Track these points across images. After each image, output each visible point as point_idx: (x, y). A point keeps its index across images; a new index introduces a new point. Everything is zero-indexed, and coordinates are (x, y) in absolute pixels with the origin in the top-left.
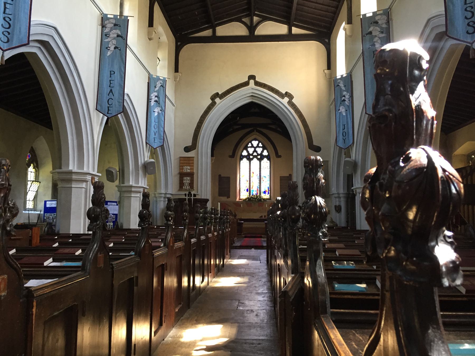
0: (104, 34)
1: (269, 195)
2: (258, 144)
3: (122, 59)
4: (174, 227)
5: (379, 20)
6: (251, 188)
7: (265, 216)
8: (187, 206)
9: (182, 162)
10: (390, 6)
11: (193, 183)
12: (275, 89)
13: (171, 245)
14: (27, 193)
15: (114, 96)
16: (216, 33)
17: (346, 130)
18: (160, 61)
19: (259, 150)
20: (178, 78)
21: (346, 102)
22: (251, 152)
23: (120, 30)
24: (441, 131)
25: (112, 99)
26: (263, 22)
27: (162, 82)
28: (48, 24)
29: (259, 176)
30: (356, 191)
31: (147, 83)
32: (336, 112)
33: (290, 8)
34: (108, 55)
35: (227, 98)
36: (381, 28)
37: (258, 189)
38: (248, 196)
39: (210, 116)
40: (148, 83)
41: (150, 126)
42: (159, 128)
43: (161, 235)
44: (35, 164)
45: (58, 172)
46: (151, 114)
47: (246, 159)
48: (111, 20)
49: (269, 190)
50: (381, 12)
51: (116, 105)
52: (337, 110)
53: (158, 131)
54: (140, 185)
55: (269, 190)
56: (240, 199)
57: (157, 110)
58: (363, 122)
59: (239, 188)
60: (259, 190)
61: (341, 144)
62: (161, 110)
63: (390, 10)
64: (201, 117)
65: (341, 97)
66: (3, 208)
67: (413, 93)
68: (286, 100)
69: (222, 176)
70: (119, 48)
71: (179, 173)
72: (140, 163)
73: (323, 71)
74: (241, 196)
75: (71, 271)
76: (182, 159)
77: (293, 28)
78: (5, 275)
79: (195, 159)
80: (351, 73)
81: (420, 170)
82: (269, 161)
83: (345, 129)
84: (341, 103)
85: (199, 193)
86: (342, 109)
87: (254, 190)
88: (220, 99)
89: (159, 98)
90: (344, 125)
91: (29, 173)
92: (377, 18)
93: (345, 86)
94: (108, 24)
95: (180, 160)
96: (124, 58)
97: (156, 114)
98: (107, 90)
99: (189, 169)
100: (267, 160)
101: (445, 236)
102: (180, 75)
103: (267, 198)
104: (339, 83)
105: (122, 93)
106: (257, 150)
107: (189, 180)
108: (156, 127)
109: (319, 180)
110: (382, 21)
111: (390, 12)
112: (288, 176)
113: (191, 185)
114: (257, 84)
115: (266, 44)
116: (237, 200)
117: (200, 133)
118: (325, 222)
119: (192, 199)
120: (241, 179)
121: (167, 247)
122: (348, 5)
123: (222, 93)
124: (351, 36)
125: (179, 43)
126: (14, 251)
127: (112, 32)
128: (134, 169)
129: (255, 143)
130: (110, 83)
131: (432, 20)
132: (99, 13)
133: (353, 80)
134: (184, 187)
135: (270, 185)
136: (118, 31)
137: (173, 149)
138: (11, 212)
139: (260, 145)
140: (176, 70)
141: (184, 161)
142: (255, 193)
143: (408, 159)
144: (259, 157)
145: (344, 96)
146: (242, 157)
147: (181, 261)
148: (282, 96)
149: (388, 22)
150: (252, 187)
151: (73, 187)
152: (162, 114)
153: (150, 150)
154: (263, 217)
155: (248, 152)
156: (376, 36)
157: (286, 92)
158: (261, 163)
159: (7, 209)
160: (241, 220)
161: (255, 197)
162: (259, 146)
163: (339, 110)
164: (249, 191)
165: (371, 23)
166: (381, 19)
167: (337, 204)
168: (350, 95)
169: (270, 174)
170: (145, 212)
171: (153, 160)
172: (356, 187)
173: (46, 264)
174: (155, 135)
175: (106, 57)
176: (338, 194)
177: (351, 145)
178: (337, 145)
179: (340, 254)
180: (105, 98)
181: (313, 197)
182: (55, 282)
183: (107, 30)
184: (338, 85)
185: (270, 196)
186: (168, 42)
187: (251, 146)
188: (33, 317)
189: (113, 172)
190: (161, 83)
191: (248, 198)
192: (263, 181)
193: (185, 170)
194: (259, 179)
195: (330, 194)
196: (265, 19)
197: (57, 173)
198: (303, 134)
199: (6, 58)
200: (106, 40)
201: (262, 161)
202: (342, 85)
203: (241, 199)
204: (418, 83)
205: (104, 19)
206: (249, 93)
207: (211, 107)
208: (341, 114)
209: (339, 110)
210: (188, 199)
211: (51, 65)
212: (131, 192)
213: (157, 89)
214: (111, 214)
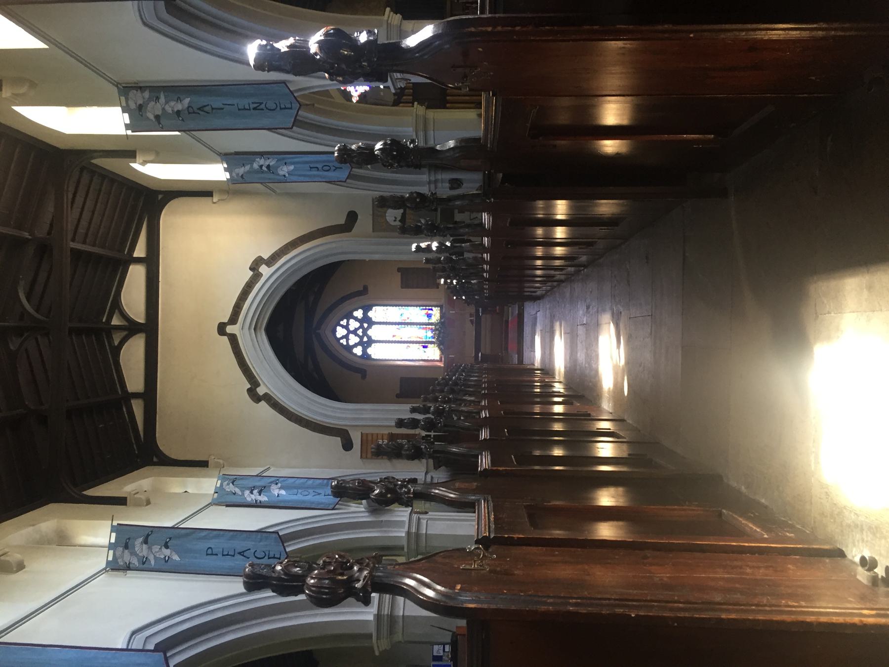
0: (141, 566)
1: (433, 308)
2: (343, 326)
3: (187, 535)
5: (136, 104)
6: (421, 340)
8: (428, 396)
10: (114, 84)
15: (250, 549)
16: (138, 391)
17: (320, 166)
19: (353, 325)
20: (219, 460)
21: (271, 164)
22: (357, 340)
23: (135, 539)
24: (324, 11)
25: (256, 551)
26: (121, 307)
28: (127, 640)
29: (400, 326)
32: (288, 181)
33: (100, 257)
35: (257, 374)
36: (150, 99)
37: (424, 328)
40: (227, 506)
41: (304, 502)
42: (308, 487)
45: (377, 639)
46: (281, 501)
48: (118, 553)
49: (424, 308)
50: (123, 98)
51: (266, 545)
52: (284, 180)
53: (313, 488)
54: (406, 519)
55: (424, 308)
56: (440, 361)
57: (275, 491)
58: (308, 136)
59: (421, 362)
60: (425, 326)
62: (277, 484)
63: (120, 84)
65: (263, 172)
67: (280, 50)
68: (264, 270)
70: (168, 540)
73: (214, 205)
74: (436, 359)
76: (364, 455)
77: (136, 255)
80: (221, 153)
81: (320, 48)
82: (374, 308)
84: (273, 173)
86: (284, 170)
87: (425, 335)
88: (259, 385)
89: (254, 487)
90: (311, 168)
92: (133, 106)
94: (124, 559)
95: (366, 458)
97: (283, 492)
100: (371, 311)
101: (357, 36)
103: (439, 312)
106: (354, 329)
108: (306, 493)
109: (359, 147)
110: (138, 98)
111: (124, 85)
112: (400, 273)
114: (233, 320)
115: (162, 309)
116: (443, 365)
118: (400, 141)
119: (434, 435)
120: (405, 358)
122: (101, 157)
123: (249, 382)
124: (157, 153)
125: (155, 459)
127: (138, 553)
128: (379, 529)
129: (340, 332)
130: (228, 555)
131: (144, 19)
132: (104, 575)
133: (232, 151)
135: (417, 306)
136: (136, 543)
137: (345, 470)
139: (344, 322)
140: (204, 464)
142: (430, 334)
143: (316, 54)
144: (366, 325)
145: (261, 166)
146: (366, 356)
148: (257, 276)
149: (140, 88)
150: (420, 338)
151: (403, 612)
152: (284, 481)
153: (345, 503)
154: (473, 318)
155: (356, 345)
156: (163, 109)
157: (251, 269)
158: (376, 321)
160: (476, 356)
161: (437, 332)
162: (345, 324)
163: (284, 176)
164: (426, 345)
165: (142, 116)
166: (134, 99)
167: (447, 185)
168: (260, 156)
169: (396, 306)
174: (319, 494)
175: (182, 562)
176: (429, 183)
178: (345, 181)
181: (376, 153)
183: (135, 562)
184: (242, 176)
186: (153, 478)
187: (345, 340)
188: (509, 470)
190: (228, 484)
191: (439, 346)
192: (408, 318)
194: (406, 326)
196: (117, 305)
197: (379, 641)
200: (153, 562)
201: (374, 319)
202: (241, 171)
203: (441, 358)
204: (274, 47)
205: (115, 567)
206: (250, 335)
208: (291, 173)
209: (284, 176)
212: (418, 535)
213: (237, 490)
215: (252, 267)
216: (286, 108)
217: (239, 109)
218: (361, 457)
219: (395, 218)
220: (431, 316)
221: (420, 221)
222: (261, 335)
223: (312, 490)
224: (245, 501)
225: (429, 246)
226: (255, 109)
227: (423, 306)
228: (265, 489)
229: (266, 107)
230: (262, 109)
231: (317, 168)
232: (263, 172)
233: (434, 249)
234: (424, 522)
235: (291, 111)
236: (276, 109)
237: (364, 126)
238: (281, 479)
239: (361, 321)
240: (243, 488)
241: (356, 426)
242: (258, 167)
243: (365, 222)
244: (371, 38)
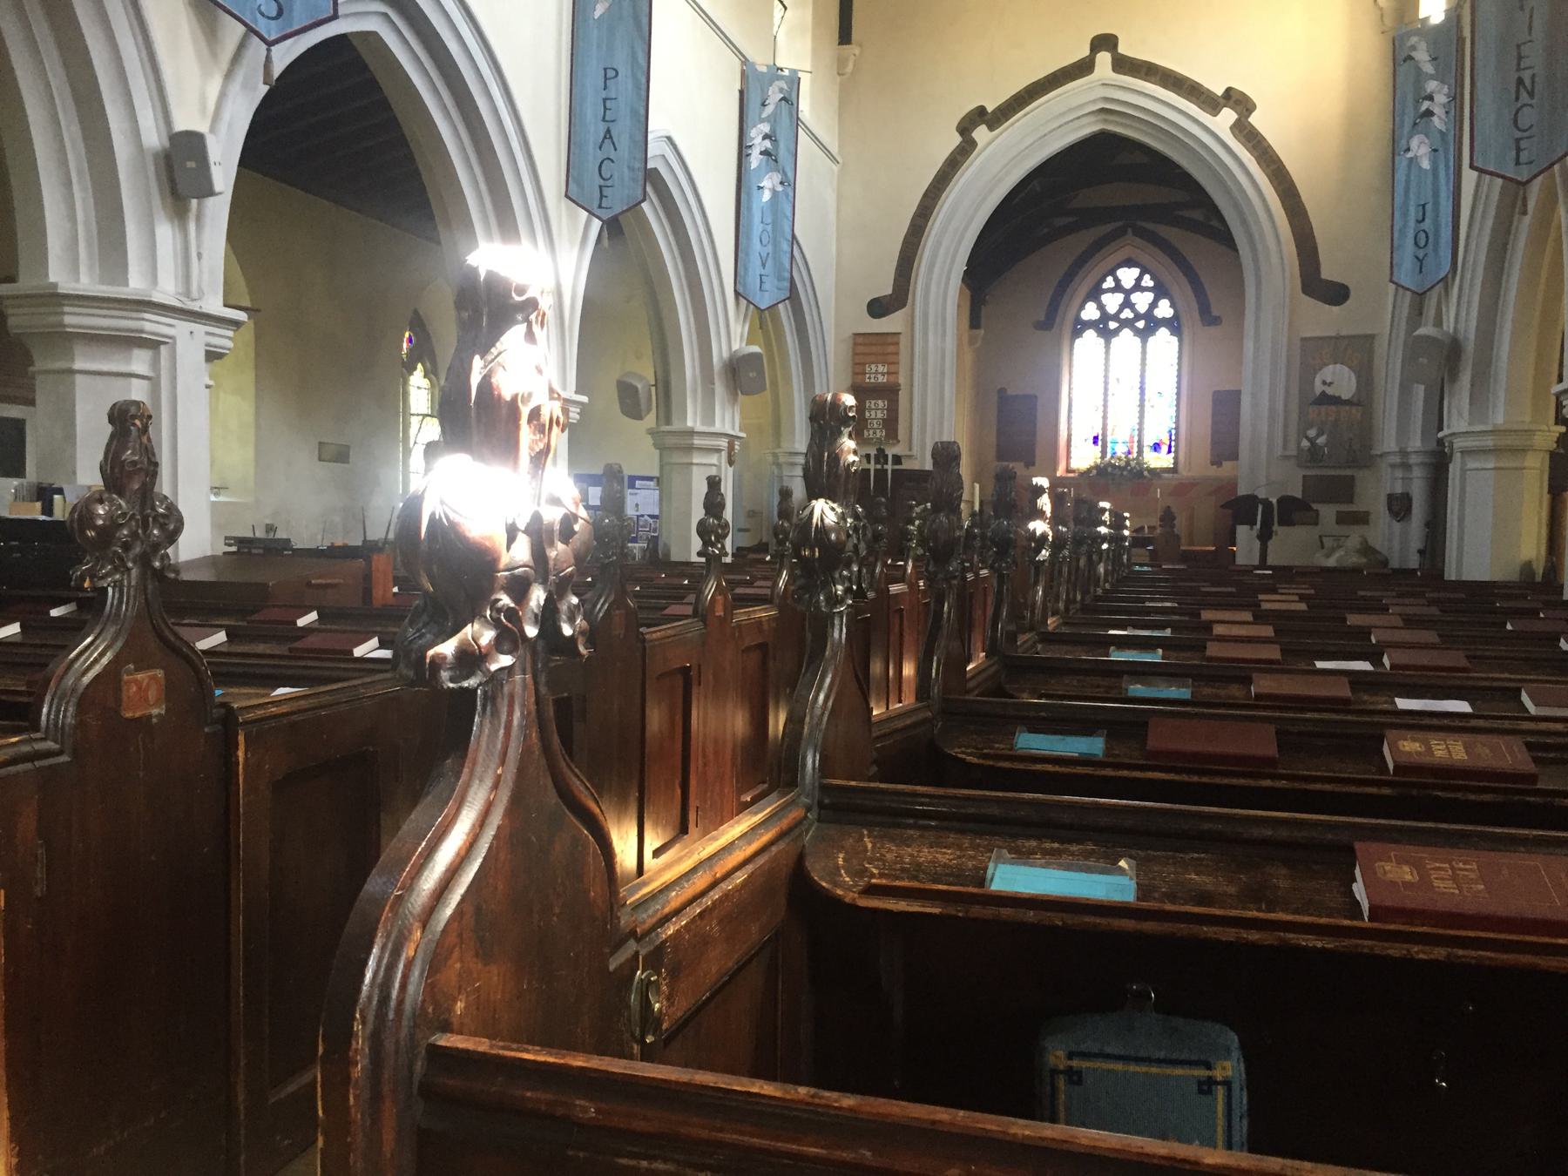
1: (1172, 455)
2: (1139, 280)
4: (889, 562)
7: (1152, 528)
9: (861, 349)
11: (896, 420)
12: (1188, 79)
13: (720, 613)
14: (410, 451)
15: (616, 149)
17: (1427, 225)
18: (786, 8)
19: (1142, 301)
21: (1435, 119)
25: (612, 161)
27: (785, 87)
30: (1451, 444)
31: (737, 95)
32: (1397, 158)
34: (597, 14)
35: (1012, 124)
37: (1132, 437)
38: (1099, 461)
39: (957, 189)
40: (741, 92)
41: (749, 238)
42: (776, 244)
43: (755, 584)
44: (428, 365)
46: (749, 195)
47: (1095, 334)
49: (1173, 438)
53: (775, 252)
54: (718, 427)
55: (1173, 438)
56: (1069, 470)
60: (1136, 439)
61: (1406, 275)
62: (782, 183)
64: (925, 195)
65: (1417, 102)
66: (138, 517)
68: (1228, 116)
69: (1011, 392)
71: (852, 386)
72: (715, 359)
75: (360, 670)
76: (860, 340)
78: (158, 671)
79: (903, 341)
82: (1175, 340)
83: (1427, 220)
84: (1415, 124)
85: (916, 451)
86: (1420, 148)
87: (1120, 441)
88: (991, 128)
90: (1424, 206)
91: (413, 391)
93: (1434, 59)
95: (855, 344)
96: (645, 20)
97: (767, 196)
98: (595, 131)
99: (883, 374)
102: (857, 51)
103: (1165, 466)
104: (1414, 48)
105: (640, 138)
106: (1133, 301)
107: (882, 409)
113: (891, 424)
114: (1124, 65)
116: (1058, 474)
117: (919, 252)
121: (704, 620)
123: (999, 109)
126: (313, 616)
129: (1128, 276)
134: (866, 433)
135: (1177, 422)
138: (162, 527)
139: (1147, 281)
140: (845, 36)
141: (868, 348)
142: (1121, 450)
144: (1141, 324)
145: (1430, 98)
146: (1080, 327)
147: (764, 664)
148: (1212, 103)
152: (787, 196)
155: (1101, 307)
157: (1229, 90)
159: (151, 519)
163: (1408, 150)
164: (1100, 443)
167: (1399, 490)
170: (607, 521)
171: (756, 349)
172: (1450, 432)
173: (358, 652)
174: (764, 265)
175: (591, 22)
176: (1404, 453)
177: (1446, 276)
179: (1397, 662)
180: (592, 157)
182: (298, 694)
184: (1410, 58)
185: (1176, 458)
189: (637, 388)
190: (781, 90)
191: (1097, 467)
193: (870, 378)
195: (1373, 452)
198: (1282, 239)
199: (278, 69)
201: (1151, 340)
202: (1422, 56)
203: (1073, 471)
206: (1094, 101)
207: (959, 157)
210: (876, 470)
211: (421, 64)
212: (690, 449)
213: (769, 110)
214: (646, 517)
215: (1232, 93)
216: (1519, 150)
217: (1518, 46)
218: (856, 335)
219: (1331, 383)
220: (1155, 450)
221: (1323, 434)
222: (1089, 124)
223: (770, 251)
224: (750, 124)
225: (1040, 514)
226: (1520, 81)
227: (1177, 434)
228: (773, 163)
229: (1522, 107)
230: (1517, 99)
231: (1423, 219)
232: (1417, 102)
233: (1032, 525)
234: (714, 459)
235: (1512, 164)
236: (1519, 129)
237: (1508, 326)
238: (790, 191)
239: (1149, 316)
240: (775, 121)
241: (913, 324)
242: (1429, 91)
243: (1323, 320)
244: (902, 563)
